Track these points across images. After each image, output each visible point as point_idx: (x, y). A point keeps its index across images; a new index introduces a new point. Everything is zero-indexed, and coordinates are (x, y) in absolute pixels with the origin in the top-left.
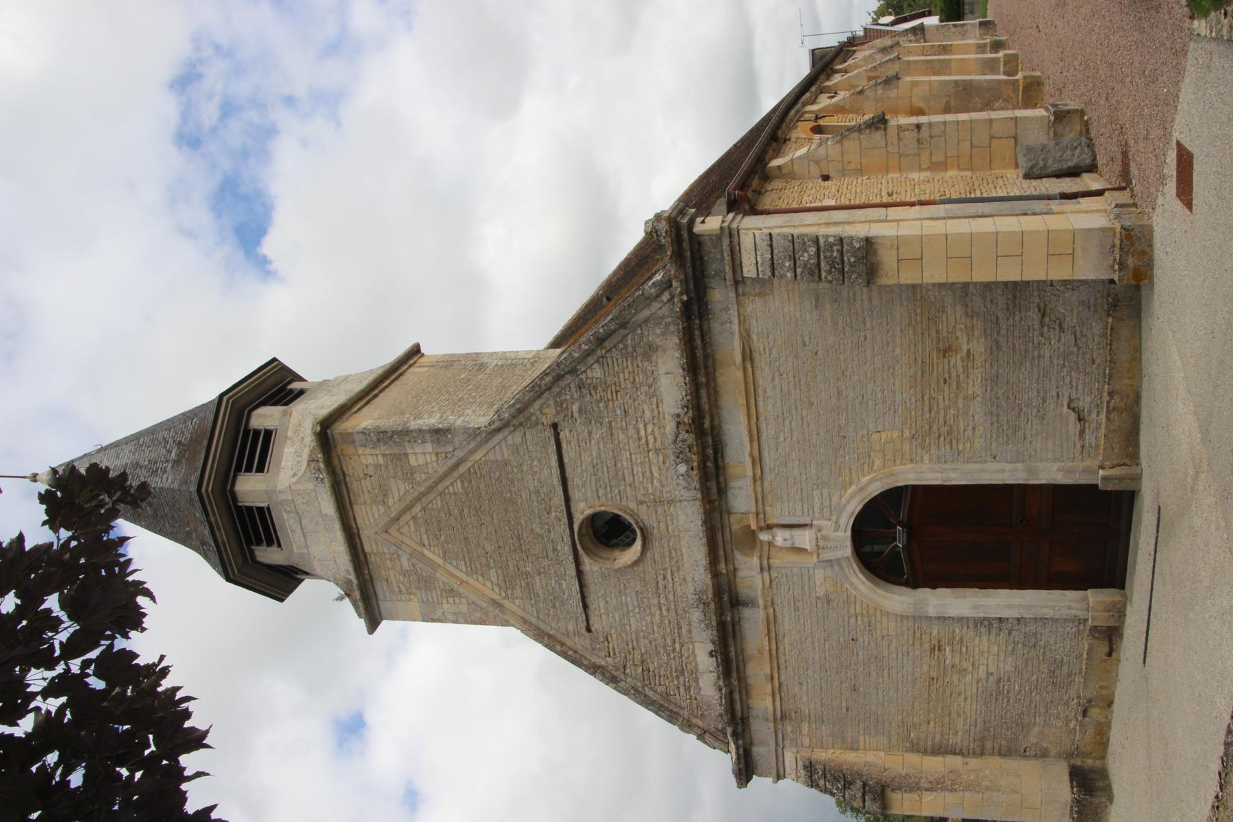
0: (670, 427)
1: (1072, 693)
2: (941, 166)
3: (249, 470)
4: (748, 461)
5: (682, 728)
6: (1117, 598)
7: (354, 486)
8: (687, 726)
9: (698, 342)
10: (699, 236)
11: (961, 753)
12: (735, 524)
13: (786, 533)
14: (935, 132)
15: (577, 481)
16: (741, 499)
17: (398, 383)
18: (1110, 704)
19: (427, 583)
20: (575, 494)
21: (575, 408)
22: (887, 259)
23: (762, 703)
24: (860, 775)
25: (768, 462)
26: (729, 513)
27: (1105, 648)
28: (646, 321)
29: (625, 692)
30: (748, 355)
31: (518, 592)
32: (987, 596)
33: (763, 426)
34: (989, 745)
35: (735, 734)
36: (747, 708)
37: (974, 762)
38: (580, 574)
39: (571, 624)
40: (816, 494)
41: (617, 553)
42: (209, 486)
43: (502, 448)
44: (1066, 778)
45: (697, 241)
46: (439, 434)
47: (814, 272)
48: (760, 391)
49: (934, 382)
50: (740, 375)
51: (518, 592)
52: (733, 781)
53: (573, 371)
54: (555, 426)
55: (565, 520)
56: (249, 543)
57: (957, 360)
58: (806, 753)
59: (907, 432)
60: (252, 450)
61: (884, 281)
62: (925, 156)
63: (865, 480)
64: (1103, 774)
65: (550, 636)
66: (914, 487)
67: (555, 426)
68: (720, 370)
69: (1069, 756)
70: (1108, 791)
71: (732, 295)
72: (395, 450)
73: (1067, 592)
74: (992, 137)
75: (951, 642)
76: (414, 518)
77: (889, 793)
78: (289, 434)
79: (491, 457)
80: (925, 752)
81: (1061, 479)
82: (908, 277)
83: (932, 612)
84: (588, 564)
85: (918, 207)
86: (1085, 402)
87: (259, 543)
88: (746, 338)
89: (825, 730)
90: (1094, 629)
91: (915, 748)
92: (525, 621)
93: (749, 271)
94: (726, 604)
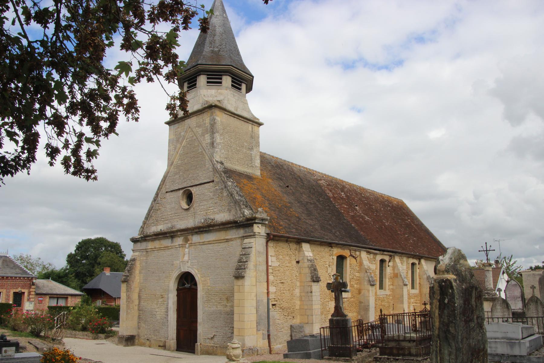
0: (212, 217)
1: (153, 336)
2: (301, 300)
3: (208, 78)
4: (203, 241)
5: (144, 221)
6: (172, 349)
7: (201, 116)
8: (144, 223)
9: (229, 226)
10: (253, 226)
11: (139, 304)
12: (190, 237)
13: (187, 252)
14: (310, 298)
15: (200, 188)
16: (196, 239)
17: (243, 122)
18: (150, 347)
19: (178, 141)
20: (198, 187)
21: (217, 187)
22: (240, 282)
23: (150, 245)
24: (131, 275)
25: (204, 247)
26: (192, 235)
27: (161, 345)
28: (236, 209)
29: (152, 204)
30: (227, 240)
31: (176, 170)
32: (174, 311)
33: (212, 245)
34: (141, 312)
35: (142, 237)
36: (149, 240)
37: (136, 308)
38: (179, 189)
39: (169, 186)
40: (196, 261)
41: (185, 200)
42: (200, 67)
43: (208, 165)
44: (131, 334)
45: (251, 225)
46: (212, 144)
47: (240, 261)
48: (219, 244)
49: (220, 295)
50: (223, 238)
51: (176, 170)
52: (131, 237)
53: (225, 187)
54: (213, 181)
55: (192, 185)
56: (188, 80)
57: (225, 302)
58: (138, 259)
59: (209, 288)
60: (215, 77)
61: (235, 281)
62: (303, 294)
63: (199, 275)
64: (133, 344)
65: (165, 180)
66: (197, 290)
67: (213, 181)
68: (224, 232)
69: (138, 336)
70: (127, 345)
71: (241, 236)
72: (209, 130)
73: (175, 334)
74: (308, 316)
75: (163, 301)
76: (193, 136)
77: (126, 283)
78: (219, 91)
79: (207, 161)
80: (139, 294)
81: (198, 332)
82: (236, 288)
83: (170, 295)
84: (181, 192)
85: (266, 291)
86: (216, 339)
87: (189, 84)
88: (231, 240)
89: (144, 264)
90: (165, 342)
91: (140, 291)
92: (168, 172)
93: (246, 241)
94: (170, 234)
